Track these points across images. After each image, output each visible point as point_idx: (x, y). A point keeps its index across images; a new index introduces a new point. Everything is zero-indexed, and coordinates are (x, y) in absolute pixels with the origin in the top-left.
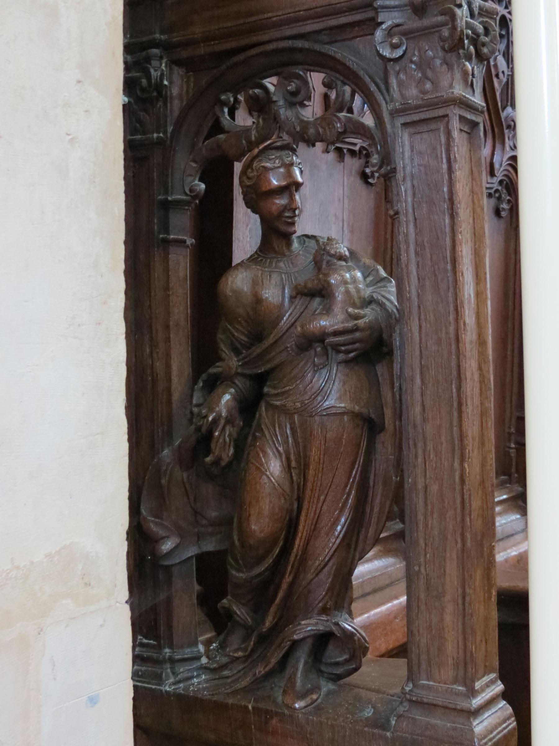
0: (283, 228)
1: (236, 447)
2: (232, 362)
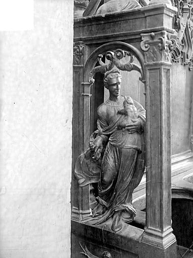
0: (116, 95)
1: (101, 155)
2: (100, 129)
